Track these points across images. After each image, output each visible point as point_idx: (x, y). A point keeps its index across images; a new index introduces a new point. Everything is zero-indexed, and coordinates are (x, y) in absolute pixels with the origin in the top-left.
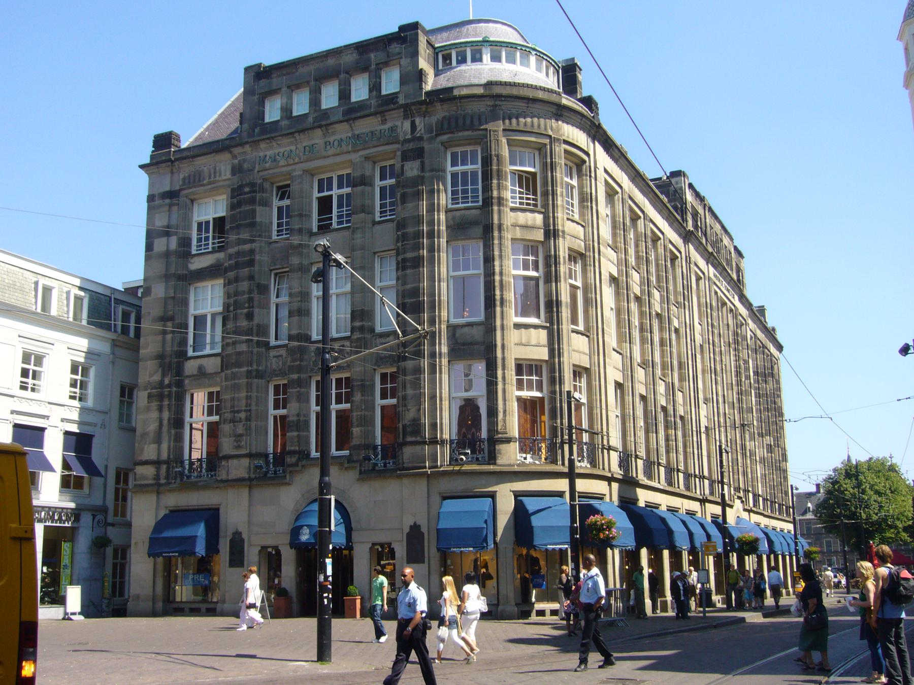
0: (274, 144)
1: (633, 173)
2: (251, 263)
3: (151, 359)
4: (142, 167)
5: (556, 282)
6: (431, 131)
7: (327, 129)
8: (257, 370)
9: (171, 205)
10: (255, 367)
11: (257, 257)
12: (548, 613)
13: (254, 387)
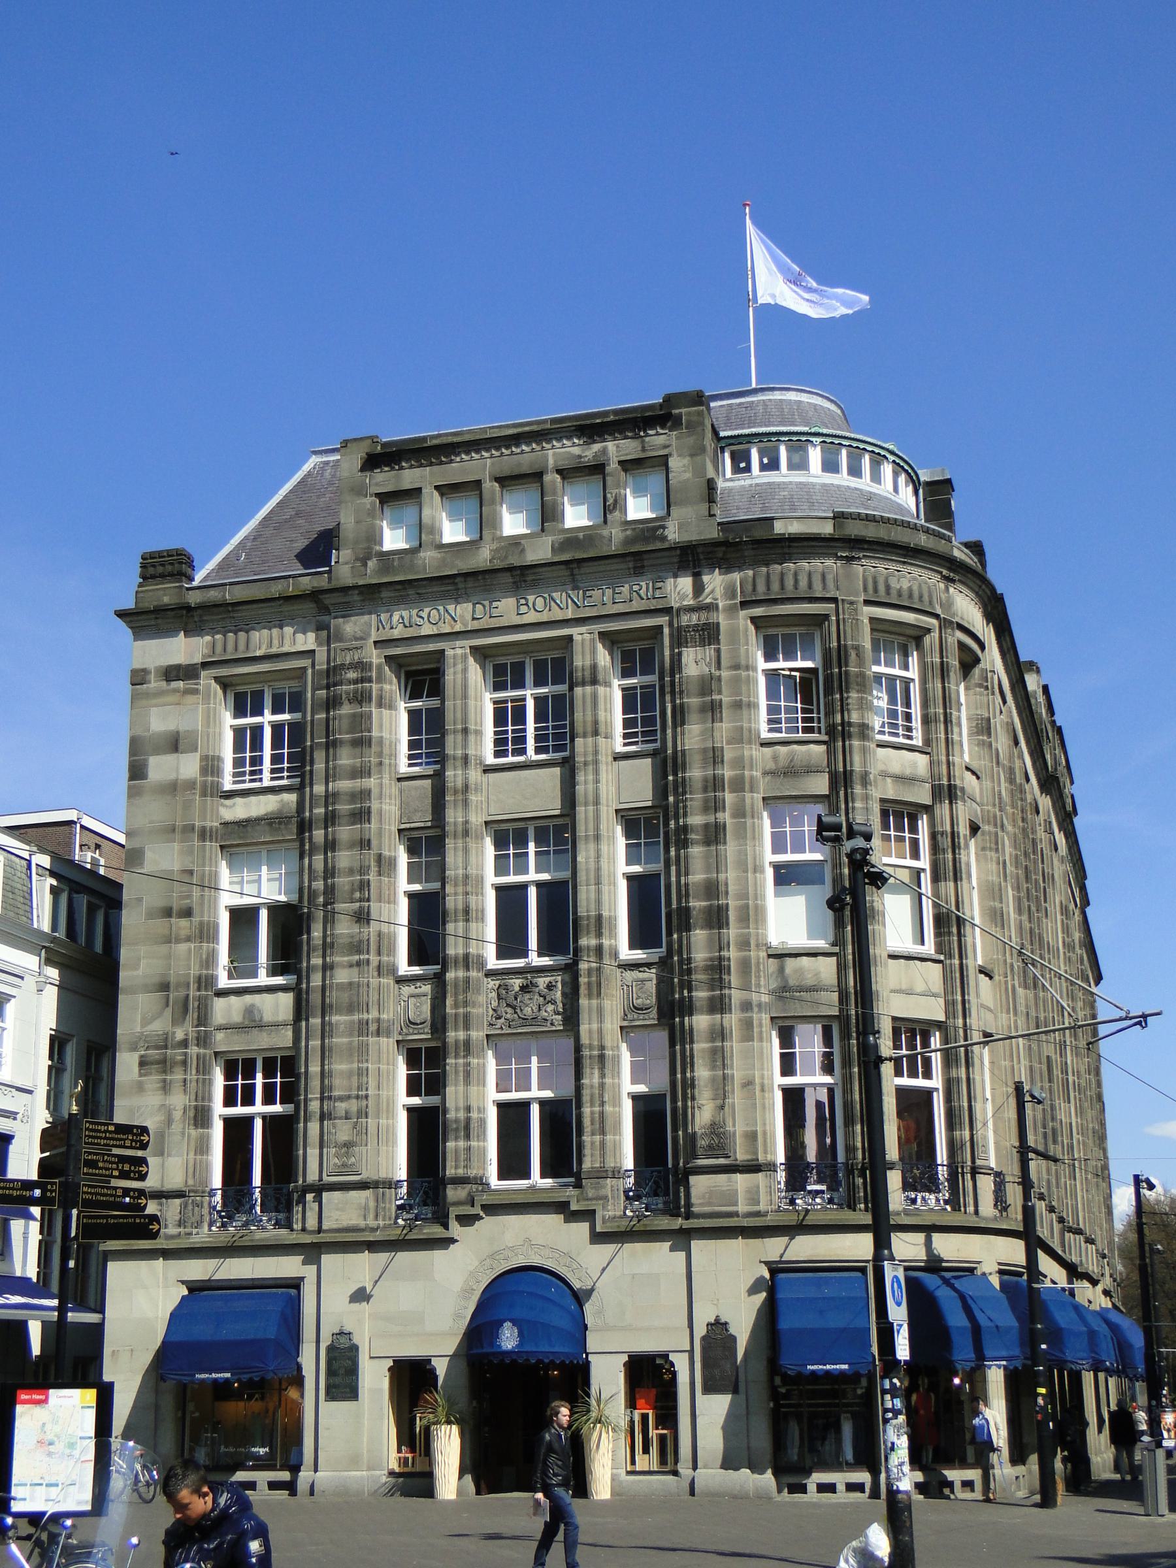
0: (411, 592)
1: (507, 578)
3: (147, 989)
4: (121, 614)
5: (956, 880)
6: (734, 596)
7: (523, 575)
8: (378, 1020)
12: (841, 1487)
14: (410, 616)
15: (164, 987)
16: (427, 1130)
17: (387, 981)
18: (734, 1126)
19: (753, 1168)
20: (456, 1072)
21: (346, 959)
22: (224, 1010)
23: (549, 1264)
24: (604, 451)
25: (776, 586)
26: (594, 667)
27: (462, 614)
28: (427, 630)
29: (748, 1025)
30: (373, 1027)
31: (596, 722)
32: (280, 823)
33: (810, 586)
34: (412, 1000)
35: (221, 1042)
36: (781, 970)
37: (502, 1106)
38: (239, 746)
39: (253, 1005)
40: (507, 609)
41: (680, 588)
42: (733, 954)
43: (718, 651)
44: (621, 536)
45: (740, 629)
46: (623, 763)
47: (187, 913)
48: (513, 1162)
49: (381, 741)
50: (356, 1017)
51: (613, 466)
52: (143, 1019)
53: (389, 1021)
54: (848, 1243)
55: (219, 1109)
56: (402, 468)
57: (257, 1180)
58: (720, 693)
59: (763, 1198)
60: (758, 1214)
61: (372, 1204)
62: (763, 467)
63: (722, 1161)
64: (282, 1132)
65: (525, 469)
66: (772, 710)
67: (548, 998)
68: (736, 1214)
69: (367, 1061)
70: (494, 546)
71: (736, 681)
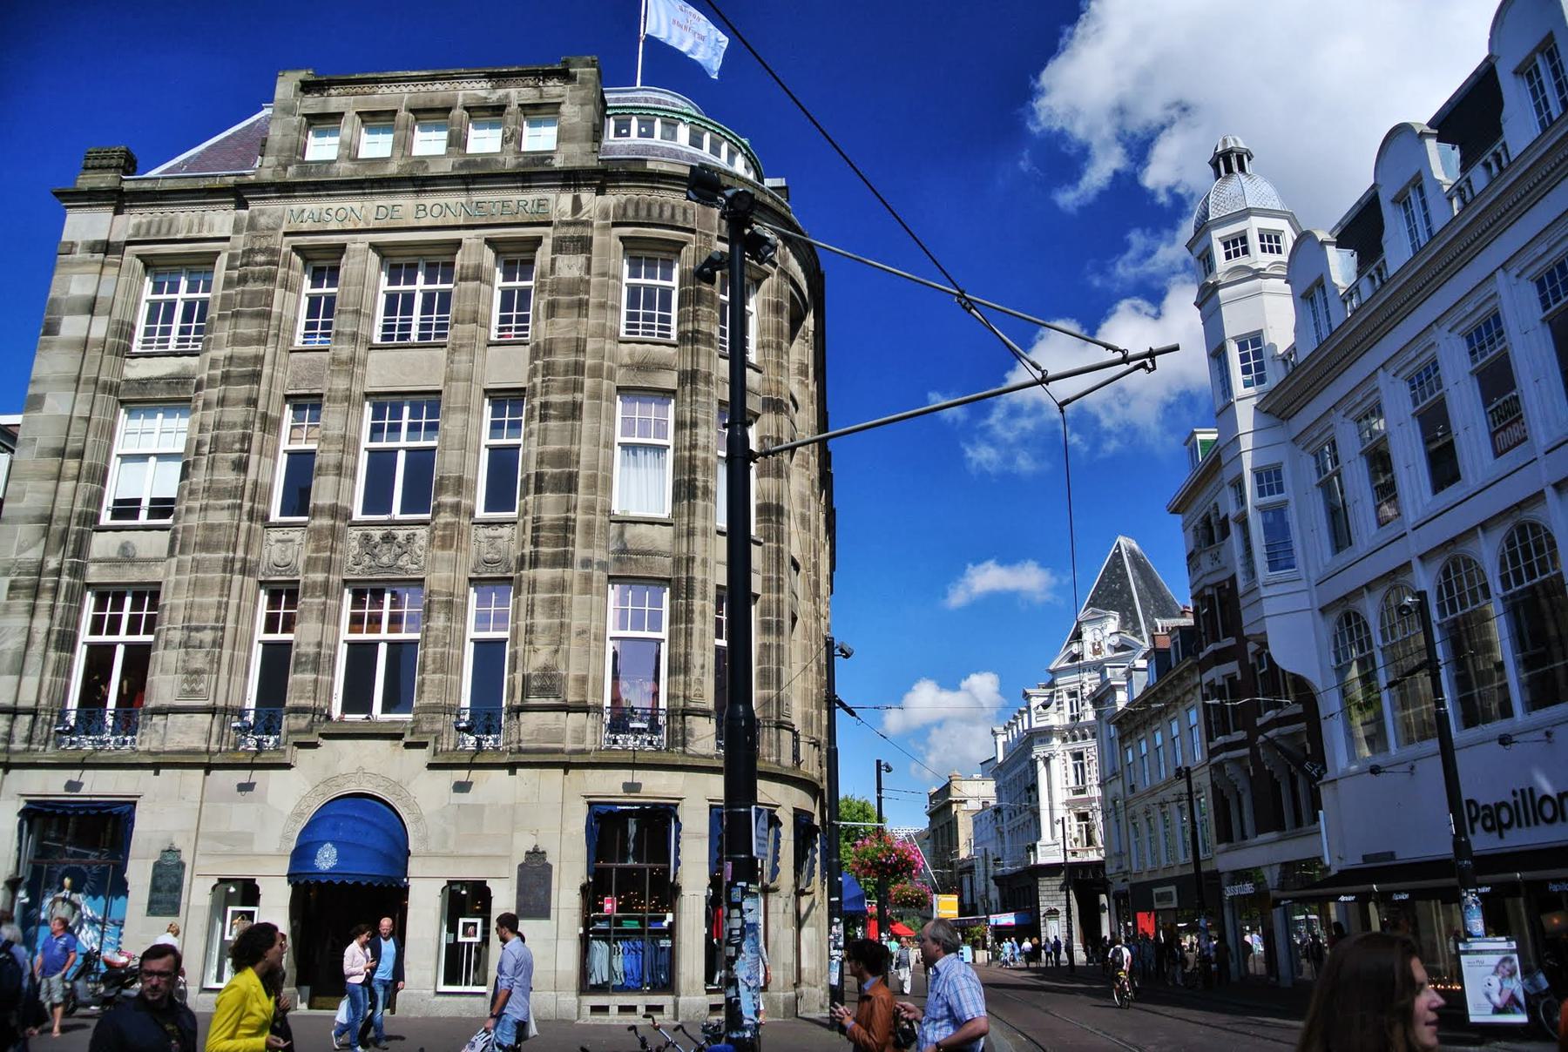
2: (255, 377)
11: (267, 370)
15: (47, 519)
16: (277, 661)
18: (567, 666)
19: (583, 708)
22: (102, 545)
23: (379, 793)
24: (507, 96)
25: (643, 213)
26: (479, 267)
29: (588, 579)
30: (238, 565)
33: (673, 215)
35: (94, 574)
36: (621, 534)
37: (352, 645)
38: (152, 318)
40: (405, 206)
41: (560, 202)
42: (580, 517)
43: (589, 260)
44: (514, 162)
45: (608, 242)
48: (357, 697)
51: (514, 107)
52: (20, 546)
54: (664, 782)
55: (85, 636)
57: (112, 702)
58: (587, 293)
59: (589, 737)
60: (583, 752)
61: (216, 729)
62: (641, 135)
63: (552, 701)
64: (138, 659)
65: (437, 104)
66: (631, 316)
68: (562, 751)
70: (402, 163)
71: (604, 286)
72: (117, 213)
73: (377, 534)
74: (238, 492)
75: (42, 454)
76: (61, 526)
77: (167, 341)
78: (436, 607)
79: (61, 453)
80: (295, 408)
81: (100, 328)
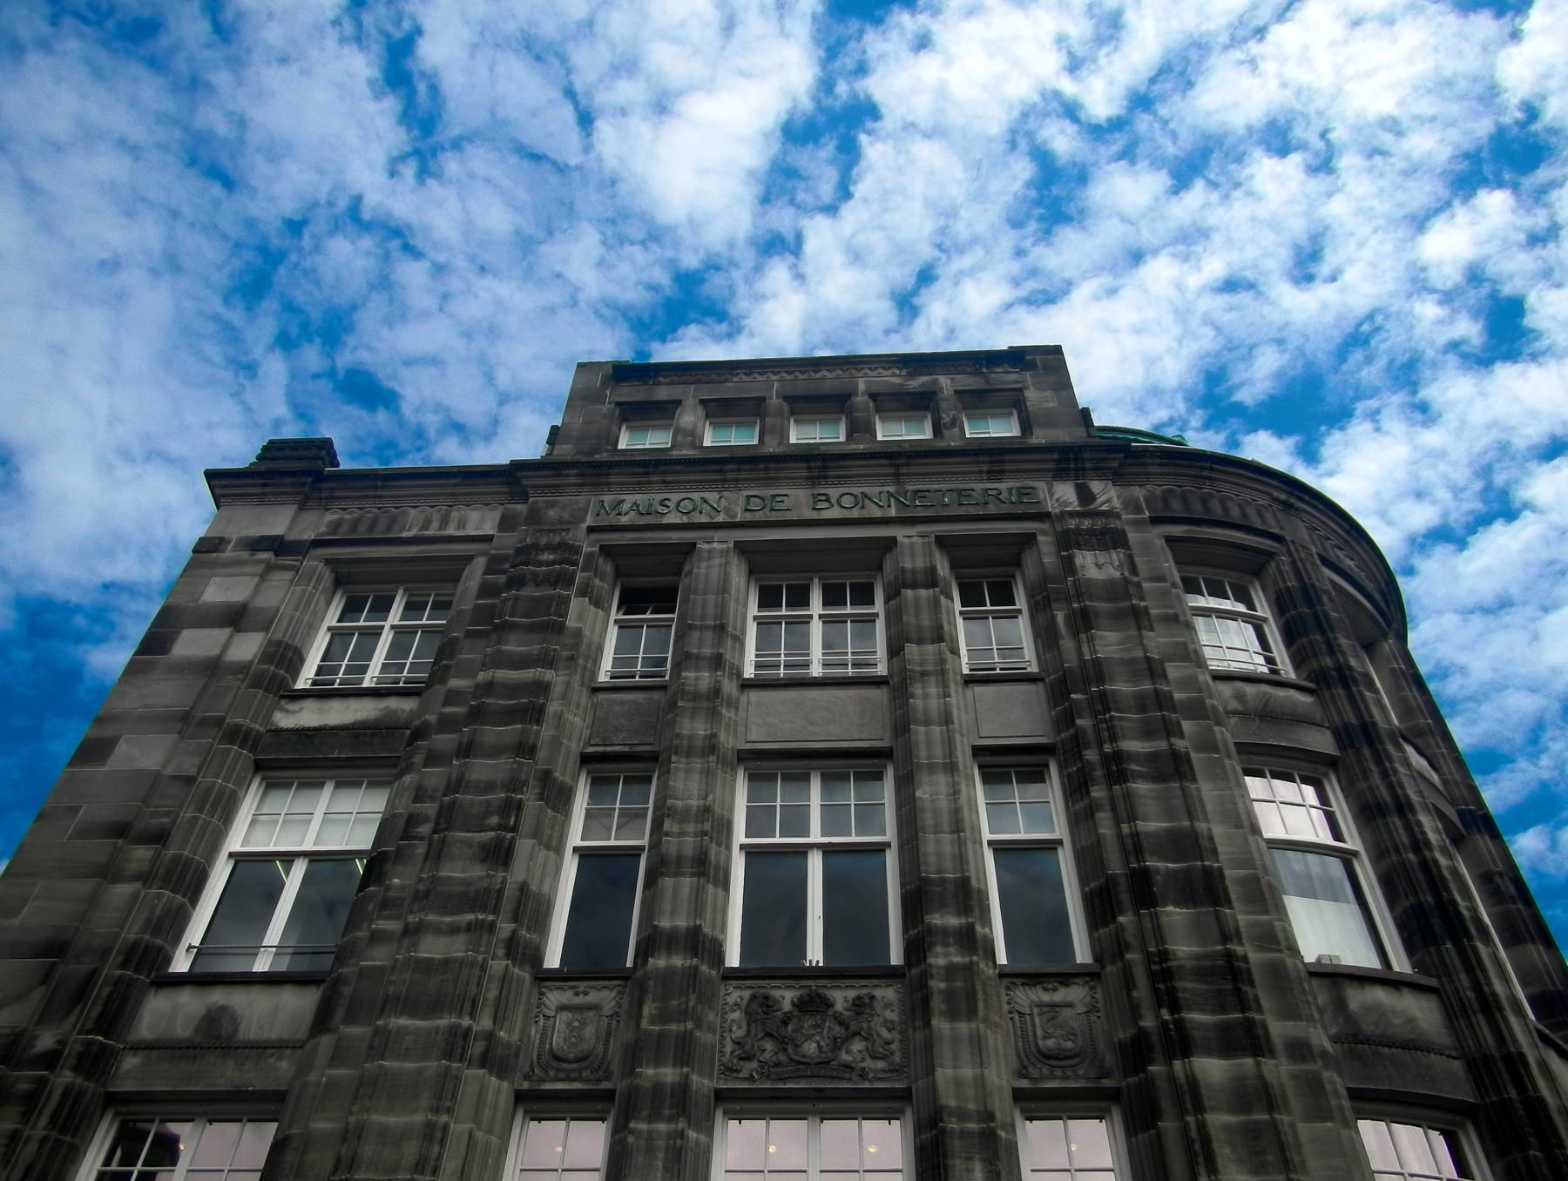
2: (536, 714)
8: (490, 1036)
9: (270, 568)
10: (485, 1022)
11: (553, 707)
13: (466, 1105)
14: (568, 684)
15: (55, 949)
17: (524, 975)
20: (650, 1151)
21: (447, 919)
27: (732, 502)
28: (673, 518)
31: (940, 628)
32: (373, 736)
34: (565, 1016)
35: (130, 1072)
39: (223, 1009)
46: (979, 689)
47: (160, 837)
49: (578, 633)
50: (443, 1022)
53: (508, 1046)
56: (659, 384)
67: (853, 1028)
69: (449, 1111)
72: (302, 508)
73: (787, 997)
74: (486, 899)
75: (84, 832)
76: (84, 968)
77: (364, 669)
78: (956, 1145)
79: (120, 831)
80: (597, 782)
81: (247, 647)
